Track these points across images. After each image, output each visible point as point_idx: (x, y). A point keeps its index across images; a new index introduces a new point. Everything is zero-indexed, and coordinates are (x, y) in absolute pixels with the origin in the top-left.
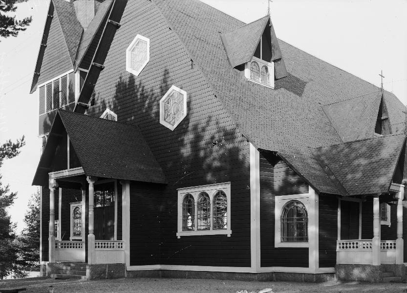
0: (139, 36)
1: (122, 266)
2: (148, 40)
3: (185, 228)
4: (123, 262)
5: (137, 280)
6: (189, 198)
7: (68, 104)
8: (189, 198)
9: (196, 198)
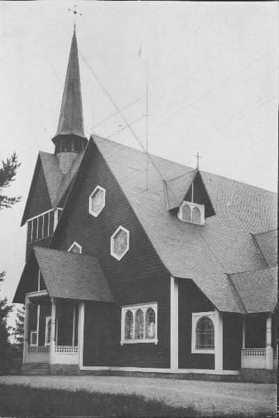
0: (98, 187)
1: (77, 366)
2: (104, 190)
3: (128, 337)
4: (77, 363)
5: (211, 411)
6: (129, 314)
7: (43, 238)
8: (129, 314)
9: (134, 312)
